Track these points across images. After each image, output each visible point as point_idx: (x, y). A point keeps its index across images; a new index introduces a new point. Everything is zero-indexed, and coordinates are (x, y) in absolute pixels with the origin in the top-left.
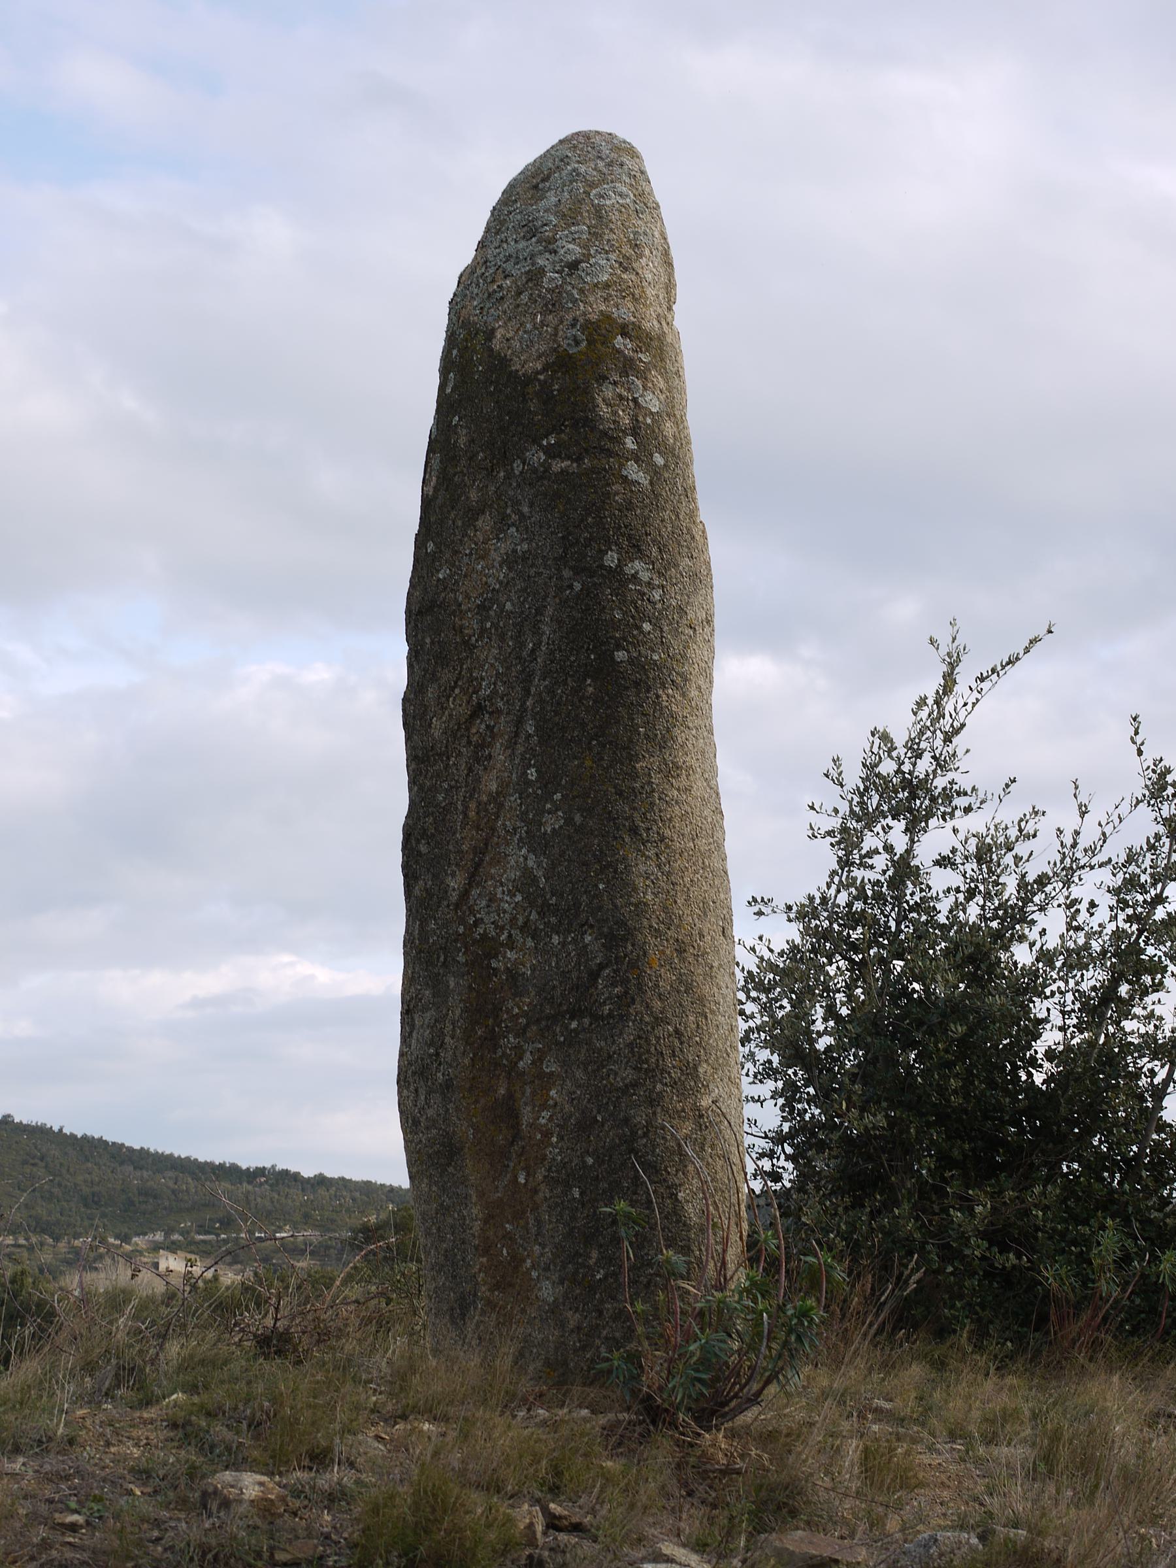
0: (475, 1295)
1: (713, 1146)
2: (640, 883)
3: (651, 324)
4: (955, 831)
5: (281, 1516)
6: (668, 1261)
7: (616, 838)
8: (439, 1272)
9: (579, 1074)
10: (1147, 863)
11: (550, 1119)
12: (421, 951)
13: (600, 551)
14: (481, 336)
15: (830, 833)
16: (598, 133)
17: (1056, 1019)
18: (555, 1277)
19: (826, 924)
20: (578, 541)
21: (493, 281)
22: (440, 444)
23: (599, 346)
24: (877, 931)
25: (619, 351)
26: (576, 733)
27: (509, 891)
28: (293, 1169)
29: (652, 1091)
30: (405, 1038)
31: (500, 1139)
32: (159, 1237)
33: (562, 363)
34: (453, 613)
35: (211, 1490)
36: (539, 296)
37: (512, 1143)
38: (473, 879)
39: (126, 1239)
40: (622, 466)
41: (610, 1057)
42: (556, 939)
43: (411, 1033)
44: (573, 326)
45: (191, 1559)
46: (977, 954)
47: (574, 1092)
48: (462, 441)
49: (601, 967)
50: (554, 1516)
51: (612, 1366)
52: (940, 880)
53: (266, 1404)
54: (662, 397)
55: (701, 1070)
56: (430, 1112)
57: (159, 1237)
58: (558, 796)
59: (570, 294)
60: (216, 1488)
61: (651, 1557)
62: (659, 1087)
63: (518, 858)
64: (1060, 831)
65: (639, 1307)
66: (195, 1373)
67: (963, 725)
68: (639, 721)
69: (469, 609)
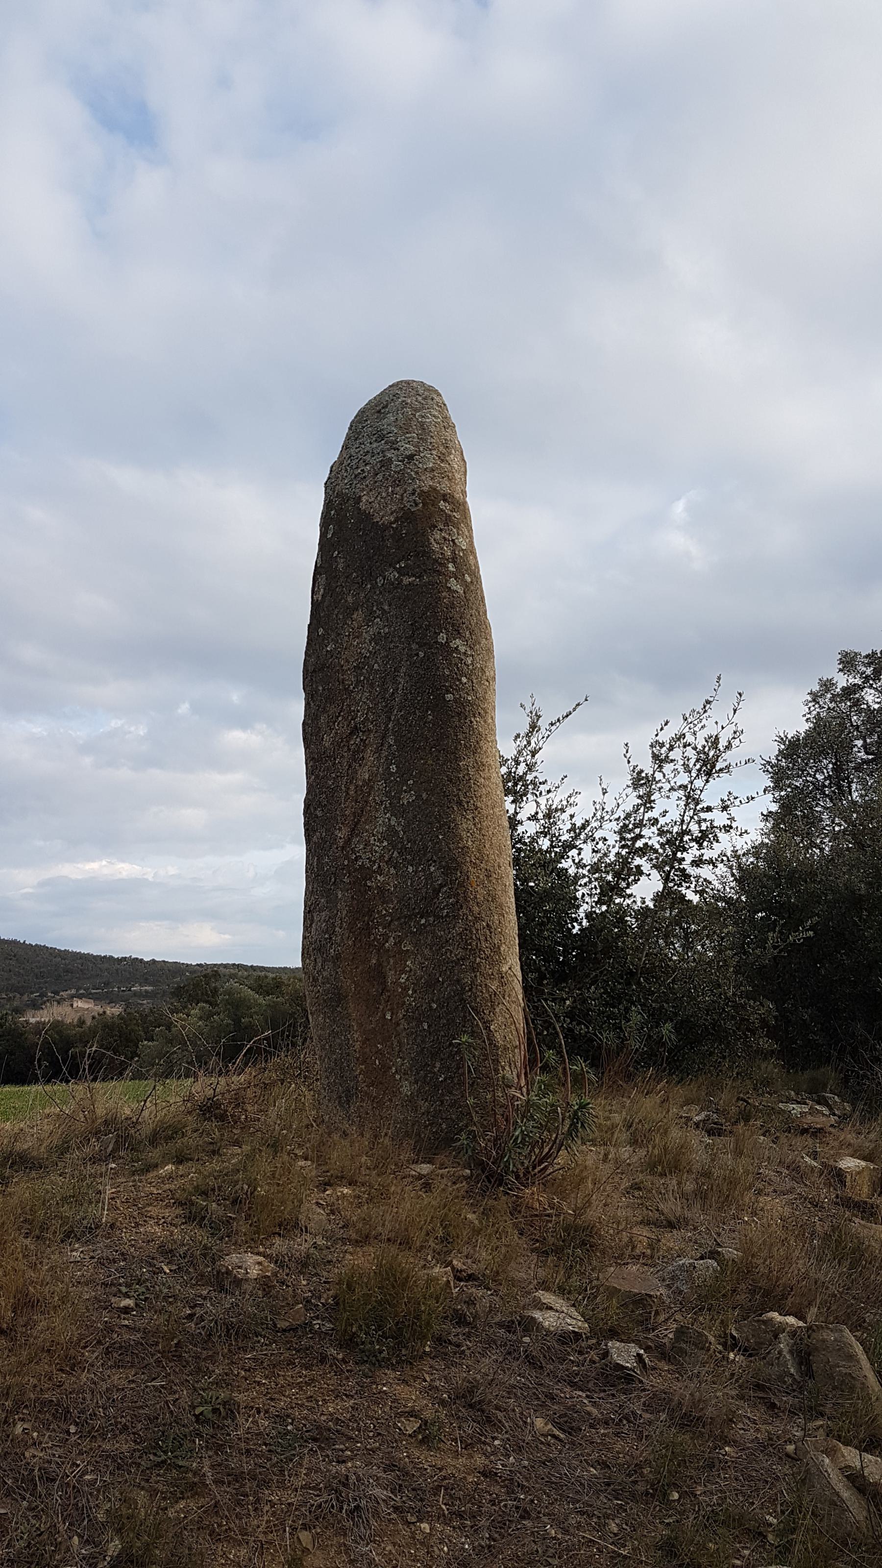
0: (357, 1089)
1: (509, 996)
9: (427, 952)
11: (407, 980)
12: (318, 875)
14: (351, 502)
20: (421, 627)
22: (325, 569)
25: (442, 510)
30: (306, 928)
32: (73, 991)
33: (407, 516)
37: (382, 994)
39: (56, 993)
40: (447, 581)
41: (447, 941)
42: (410, 869)
43: (311, 925)
44: (413, 494)
48: (340, 566)
49: (441, 886)
56: (325, 973)
57: (73, 991)
58: (411, 782)
62: (478, 959)
63: (383, 819)
67: (540, 749)
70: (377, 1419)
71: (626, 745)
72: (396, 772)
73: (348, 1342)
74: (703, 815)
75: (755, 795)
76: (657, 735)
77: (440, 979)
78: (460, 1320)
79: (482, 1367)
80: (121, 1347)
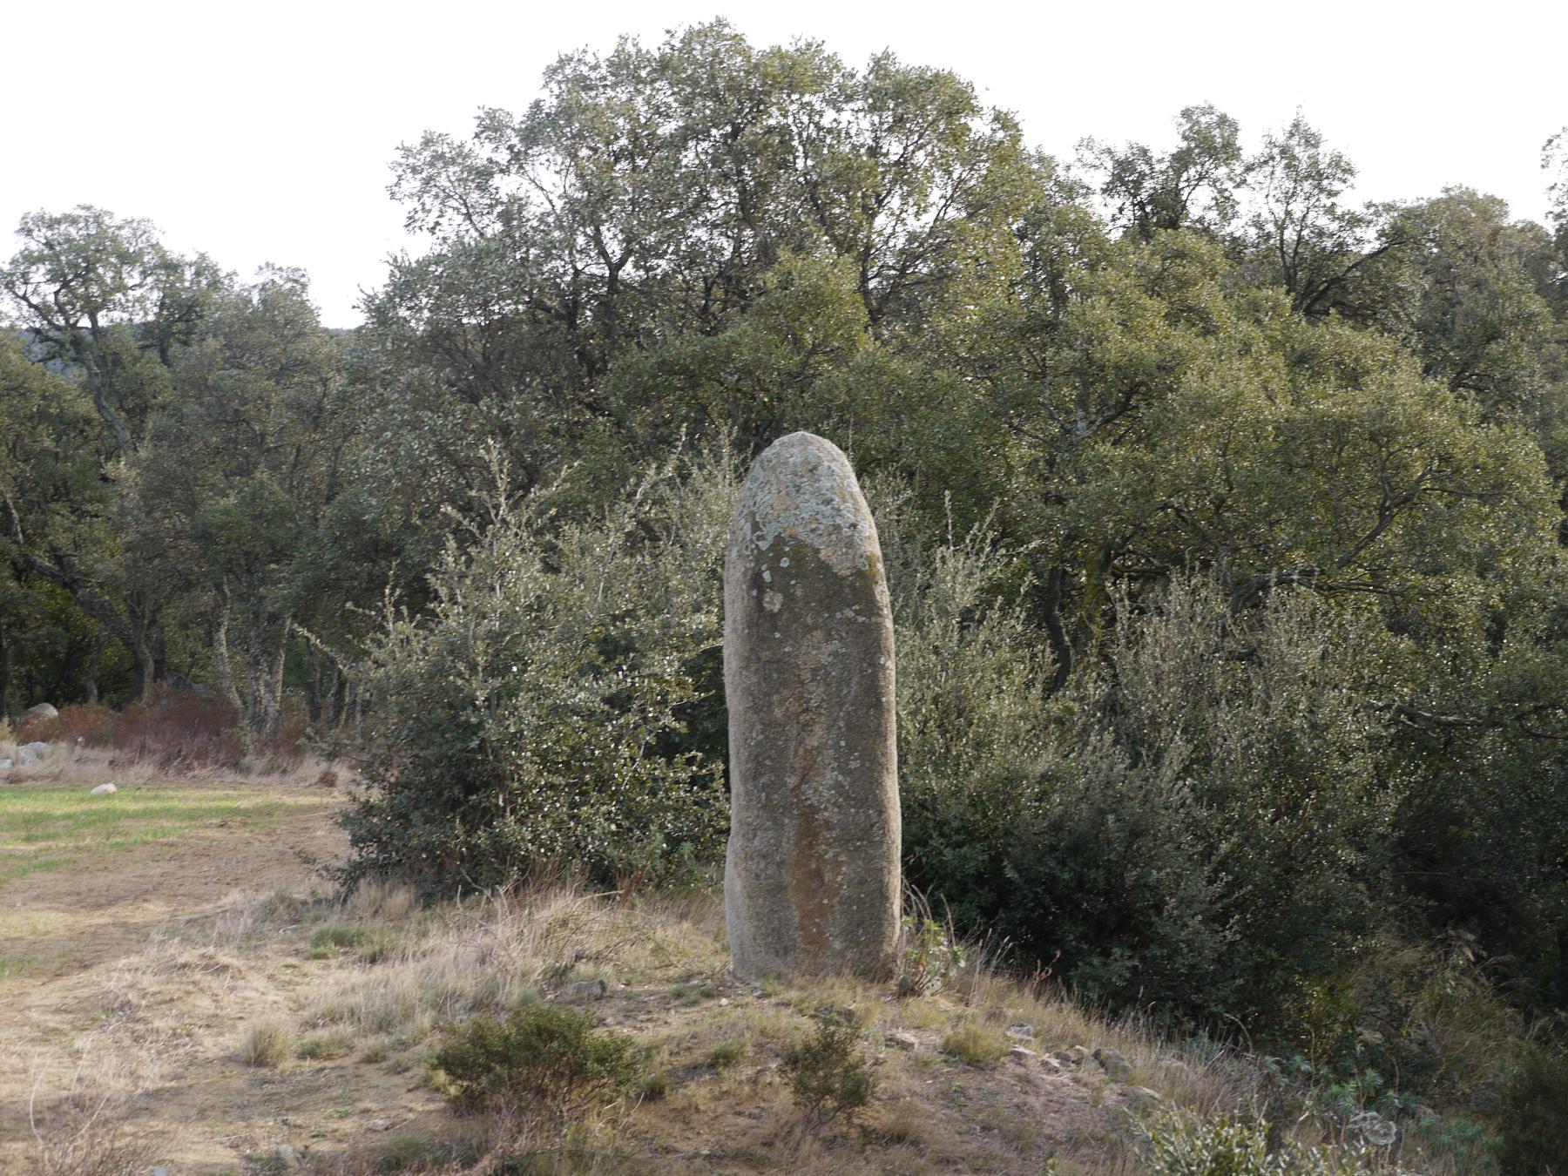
31: (814, 886)
38: (804, 779)
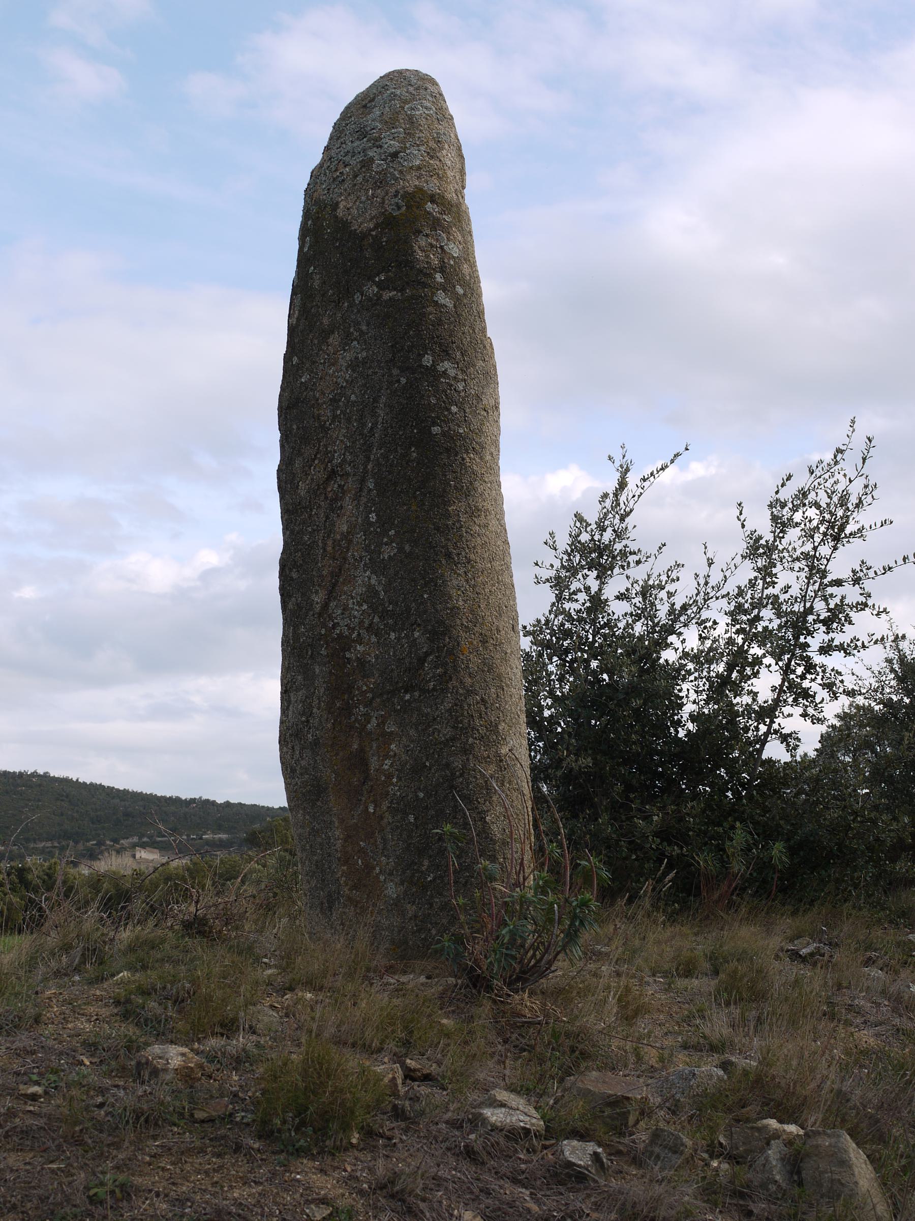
0: (339, 893)
1: (510, 782)
2: (454, 593)
3: (451, 196)
4: (628, 577)
5: (200, 1079)
6: (485, 869)
7: (435, 561)
8: (312, 877)
9: (412, 732)
10: (749, 596)
11: (391, 765)
12: (294, 648)
13: (419, 355)
14: (328, 209)
15: (547, 580)
16: (407, 70)
17: (693, 695)
18: (397, 880)
19: (548, 637)
21: (336, 170)
23: (414, 209)
24: (580, 643)
25: (429, 213)
26: (405, 487)
27: (358, 602)
28: (212, 799)
29: (466, 743)
30: (284, 710)
31: (355, 781)
32: (135, 839)
34: (313, 406)
35: (144, 1061)
36: (370, 177)
38: (331, 594)
40: (433, 294)
41: (435, 719)
43: (288, 706)
44: (396, 196)
45: (127, 1122)
46: (644, 654)
47: (409, 746)
48: (317, 284)
49: (427, 654)
50: (410, 1070)
51: (443, 946)
52: (619, 608)
53: (187, 985)
54: (461, 247)
55: (500, 727)
56: (303, 763)
57: (135, 839)
58: (392, 532)
59: (392, 174)
60: (148, 1059)
61: (488, 1102)
62: (471, 740)
64: (697, 575)
65: (461, 901)
66: (140, 955)
67: (631, 511)
68: (450, 476)
69: (324, 403)
70: (284, 1205)
71: (740, 505)
72: (376, 521)
73: (266, 1133)
74: (830, 590)
75: (892, 564)
76: (777, 492)
77: (428, 764)
78: (398, 1113)
79: (410, 1160)
80: (22, 1132)
